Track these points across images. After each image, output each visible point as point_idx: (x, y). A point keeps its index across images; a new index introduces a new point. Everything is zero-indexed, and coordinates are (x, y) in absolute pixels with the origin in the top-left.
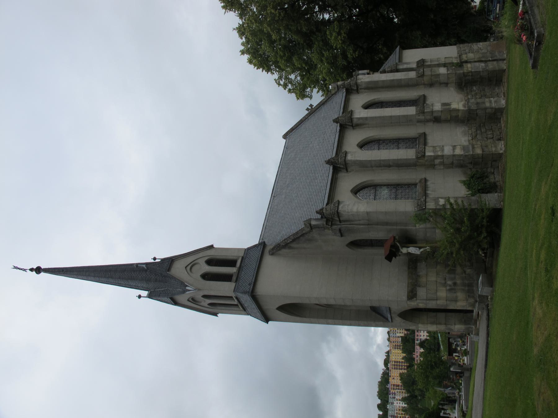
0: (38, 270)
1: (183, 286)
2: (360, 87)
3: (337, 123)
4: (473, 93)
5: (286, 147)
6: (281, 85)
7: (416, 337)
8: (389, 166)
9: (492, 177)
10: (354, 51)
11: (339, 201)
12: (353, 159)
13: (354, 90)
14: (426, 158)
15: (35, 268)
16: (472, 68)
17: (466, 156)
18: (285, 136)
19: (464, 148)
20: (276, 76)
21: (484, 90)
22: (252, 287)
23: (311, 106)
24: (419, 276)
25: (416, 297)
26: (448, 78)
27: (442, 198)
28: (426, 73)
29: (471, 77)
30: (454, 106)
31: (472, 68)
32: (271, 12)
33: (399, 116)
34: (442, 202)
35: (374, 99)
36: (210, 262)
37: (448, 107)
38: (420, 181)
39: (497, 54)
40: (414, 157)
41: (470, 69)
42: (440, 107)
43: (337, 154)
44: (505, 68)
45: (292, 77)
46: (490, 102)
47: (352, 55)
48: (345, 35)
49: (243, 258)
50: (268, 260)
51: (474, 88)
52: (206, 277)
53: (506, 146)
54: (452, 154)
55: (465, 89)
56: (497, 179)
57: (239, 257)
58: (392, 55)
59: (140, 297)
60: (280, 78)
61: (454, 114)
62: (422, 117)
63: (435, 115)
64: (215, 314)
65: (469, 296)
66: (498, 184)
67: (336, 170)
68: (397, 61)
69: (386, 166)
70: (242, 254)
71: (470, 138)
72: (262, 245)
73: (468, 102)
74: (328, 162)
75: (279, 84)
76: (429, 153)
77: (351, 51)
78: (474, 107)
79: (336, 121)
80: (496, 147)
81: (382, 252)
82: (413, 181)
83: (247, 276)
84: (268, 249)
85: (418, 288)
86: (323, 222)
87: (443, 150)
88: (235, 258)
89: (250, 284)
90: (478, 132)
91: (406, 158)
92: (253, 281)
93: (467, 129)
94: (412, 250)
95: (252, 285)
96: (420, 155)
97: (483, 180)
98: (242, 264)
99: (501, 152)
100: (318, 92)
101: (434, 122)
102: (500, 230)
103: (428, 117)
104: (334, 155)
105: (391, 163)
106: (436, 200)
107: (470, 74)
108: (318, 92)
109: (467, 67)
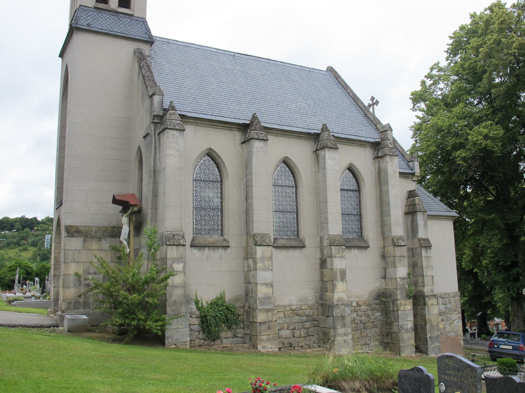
2: (381, 160)
3: (322, 129)
4: (370, 312)
5: (311, 71)
6: (431, 71)
8: (247, 199)
9: (229, 334)
10: (464, 159)
11: (184, 130)
12: (255, 149)
13: (378, 153)
14: (253, 247)
16: (404, 310)
17: (256, 300)
18: (331, 70)
20: (444, 63)
21: (375, 326)
22: (83, 27)
24: (100, 239)
25: (68, 236)
26: (391, 279)
27: (184, 267)
28: (398, 249)
29: (391, 309)
30: (340, 286)
31: (404, 310)
32: (514, 42)
33: (327, 212)
34: (179, 267)
35: (363, 180)
37: (339, 277)
38: (225, 240)
39: (437, 344)
40: (255, 231)
41: (402, 308)
42: (339, 267)
43: (265, 128)
44: (403, 355)
45: (441, 85)
46: (345, 335)
47: (458, 156)
48: (483, 145)
49: (132, 15)
50: (129, 47)
51: (378, 314)
53: (268, 354)
54: (258, 282)
55: (377, 301)
56: (225, 341)
57: (133, 11)
58: (446, 207)
60: (440, 70)
61: (329, 286)
62: (326, 243)
63: (328, 260)
65: (70, 303)
66: (218, 342)
67: (244, 128)
68: (429, 213)
69: (247, 194)
70: (136, 14)
71: (294, 307)
72: (150, 41)
73: (346, 305)
74: (254, 117)
75: (432, 69)
76: (260, 251)
77: (463, 155)
78: (337, 312)
79: (325, 128)
80: (268, 340)
82: (225, 231)
83: (103, 22)
84: (146, 49)
85: (82, 239)
86: (158, 111)
87: (264, 270)
88: (132, 6)
89: (88, 25)
90: (304, 318)
91: (255, 220)
92: (93, 29)
93: (310, 303)
94: (125, 230)
95: (87, 28)
96: (258, 239)
97: (224, 322)
98: (121, 15)
99: (259, 347)
100: (418, 117)
101: (321, 259)
102: (128, 343)
103: (326, 252)
104: (263, 124)
105: (249, 201)
106: (181, 259)
107: (395, 309)
108: (418, 117)
109: (405, 305)
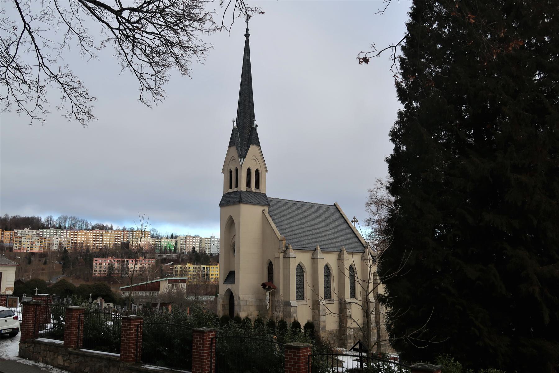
0: (247, 36)
1: (243, 155)
7: (130, 260)
15: (249, 33)
19: (324, 327)
23: (355, 221)
36: (257, 172)
46: (351, 343)
52: (249, 171)
59: (234, 121)
64: (223, 171)
81: (266, 280)
